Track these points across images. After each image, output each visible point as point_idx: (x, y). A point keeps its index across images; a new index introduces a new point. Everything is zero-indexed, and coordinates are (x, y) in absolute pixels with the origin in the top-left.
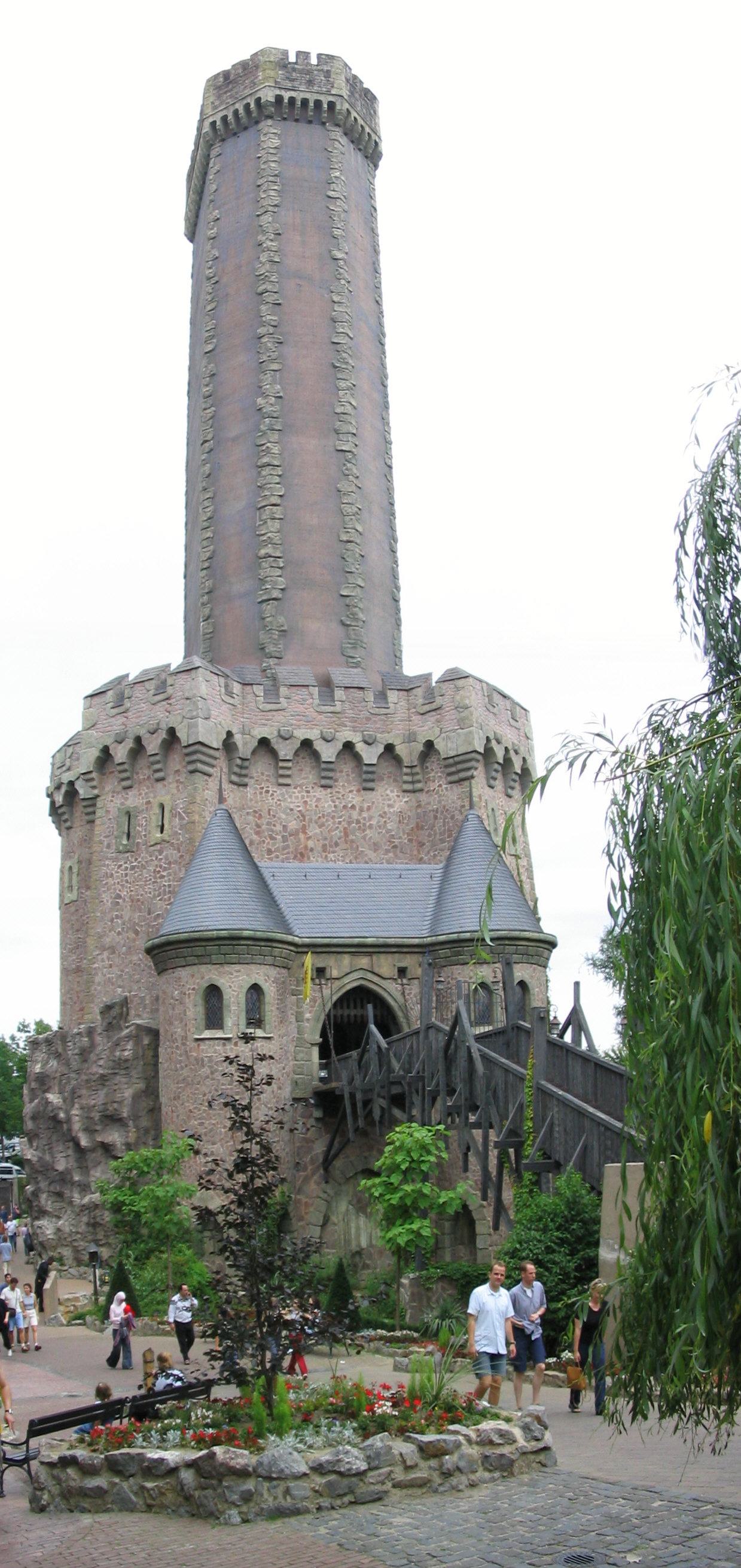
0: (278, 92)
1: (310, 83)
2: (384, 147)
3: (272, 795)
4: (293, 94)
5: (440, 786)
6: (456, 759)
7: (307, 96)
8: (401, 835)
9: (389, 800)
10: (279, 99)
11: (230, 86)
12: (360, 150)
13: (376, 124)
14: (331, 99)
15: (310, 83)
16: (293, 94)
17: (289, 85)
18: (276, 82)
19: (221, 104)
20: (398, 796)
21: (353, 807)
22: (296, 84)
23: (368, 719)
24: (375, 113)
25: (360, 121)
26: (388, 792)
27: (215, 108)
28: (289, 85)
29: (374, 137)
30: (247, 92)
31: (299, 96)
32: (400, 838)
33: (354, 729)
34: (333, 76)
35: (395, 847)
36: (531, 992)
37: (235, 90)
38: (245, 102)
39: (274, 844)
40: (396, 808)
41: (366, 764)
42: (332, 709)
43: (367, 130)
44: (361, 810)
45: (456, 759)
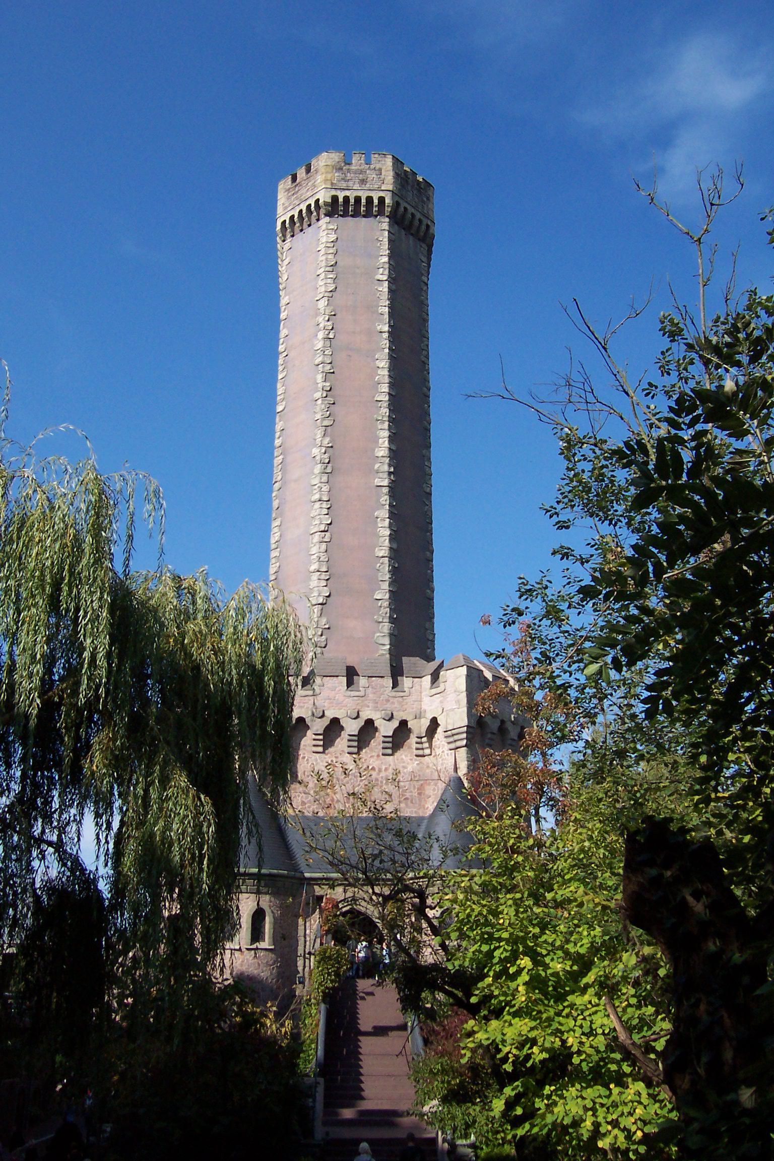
0: (334, 193)
1: (363, 182)
2: (438, 231)
3: (307, 760)
4: (347, 193)
5: (443, 752)
6: (453, 732)
7: (359, 194)
8: (412, 789)
9: (404, 762)
10: (335, 199)
11: (297, 189)
12: (412, 234)
13: (428, 209)
14: (382, 194)
15: (363, 182)
16: (347, 193)
17: (344, 185)
18: (332, 184)
19: (290, 205)
20: (411, 760)
21: (373, 769)
22: (351, 184)
23: (388, 701)
24: (428, 199)
25: (411, 210)
26: (403, 757)
27: (285, 208)
28: (344, 185)
29: (425, 221)
30: (309, 194)
31: (352, 195)
32: (411, 792)
33: (376, 709)
34: (383, 173)
35: (406, 799)
36: (256, 975)
37: (300, 193)
38: (307, 204)
39: (307, 798)
40: (410, 769)
41: (320, 746)
42: (357, 693)
43: (418, 216)
44: (380, 771)
45: (453, 732)
